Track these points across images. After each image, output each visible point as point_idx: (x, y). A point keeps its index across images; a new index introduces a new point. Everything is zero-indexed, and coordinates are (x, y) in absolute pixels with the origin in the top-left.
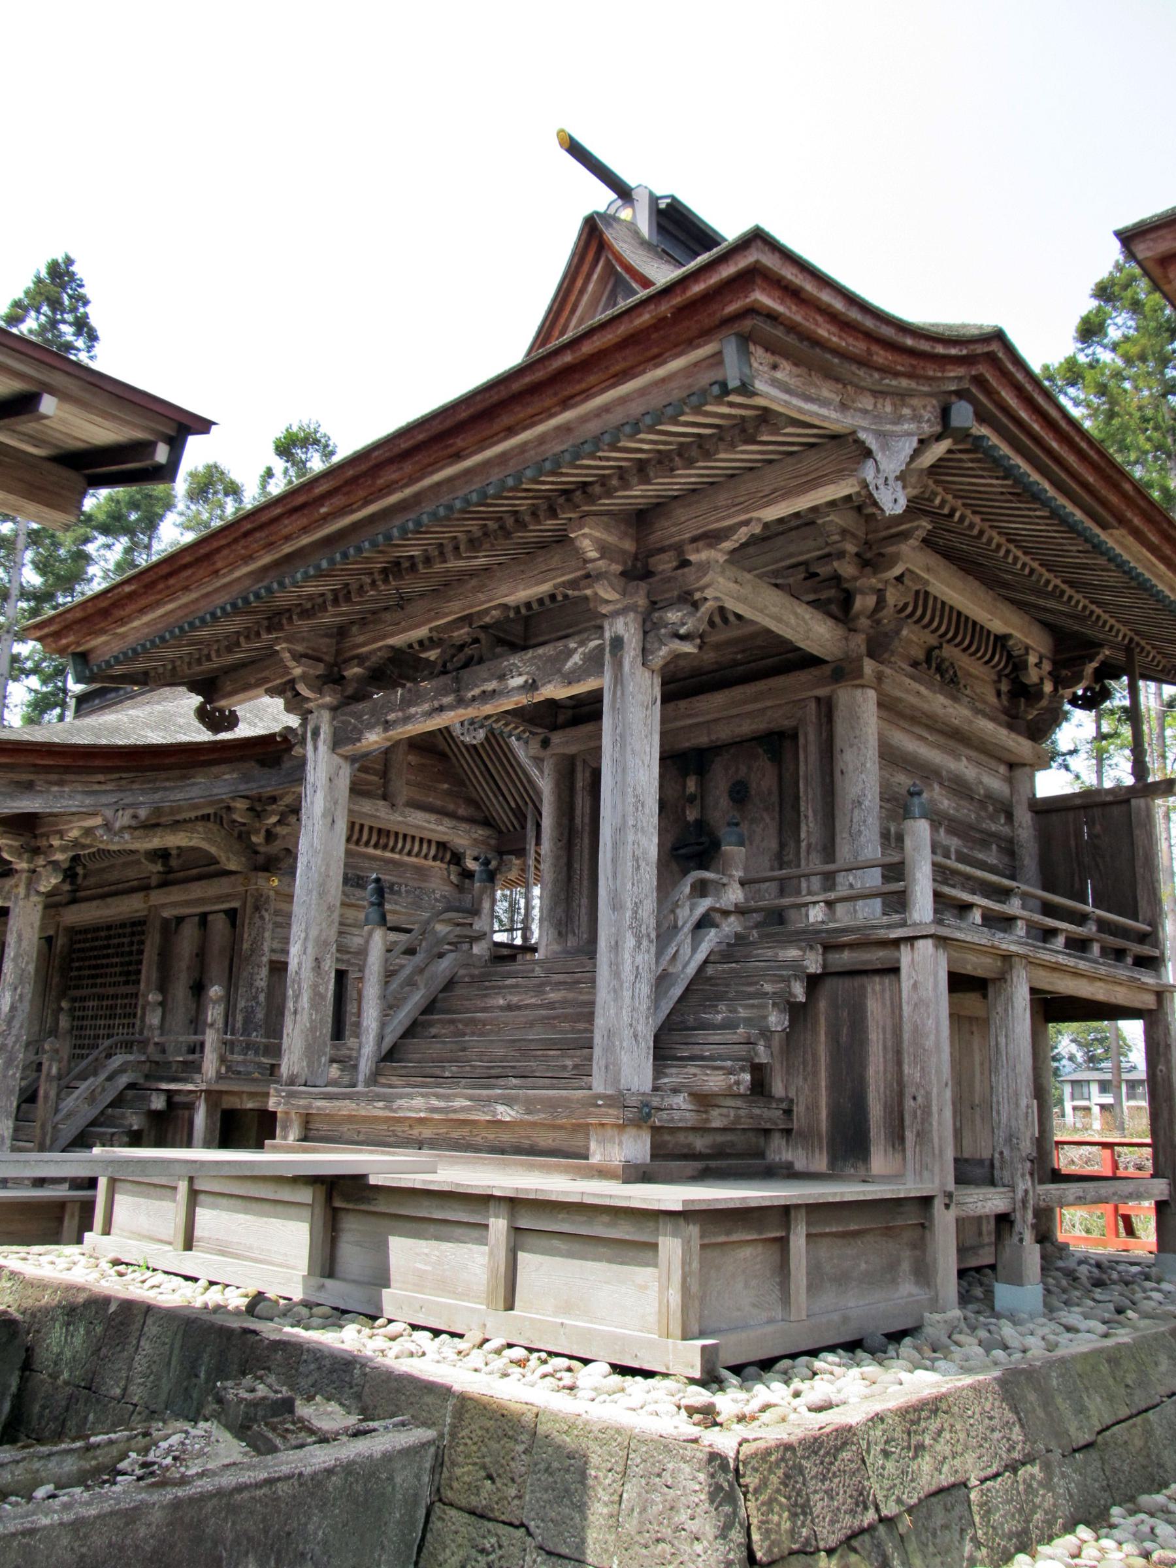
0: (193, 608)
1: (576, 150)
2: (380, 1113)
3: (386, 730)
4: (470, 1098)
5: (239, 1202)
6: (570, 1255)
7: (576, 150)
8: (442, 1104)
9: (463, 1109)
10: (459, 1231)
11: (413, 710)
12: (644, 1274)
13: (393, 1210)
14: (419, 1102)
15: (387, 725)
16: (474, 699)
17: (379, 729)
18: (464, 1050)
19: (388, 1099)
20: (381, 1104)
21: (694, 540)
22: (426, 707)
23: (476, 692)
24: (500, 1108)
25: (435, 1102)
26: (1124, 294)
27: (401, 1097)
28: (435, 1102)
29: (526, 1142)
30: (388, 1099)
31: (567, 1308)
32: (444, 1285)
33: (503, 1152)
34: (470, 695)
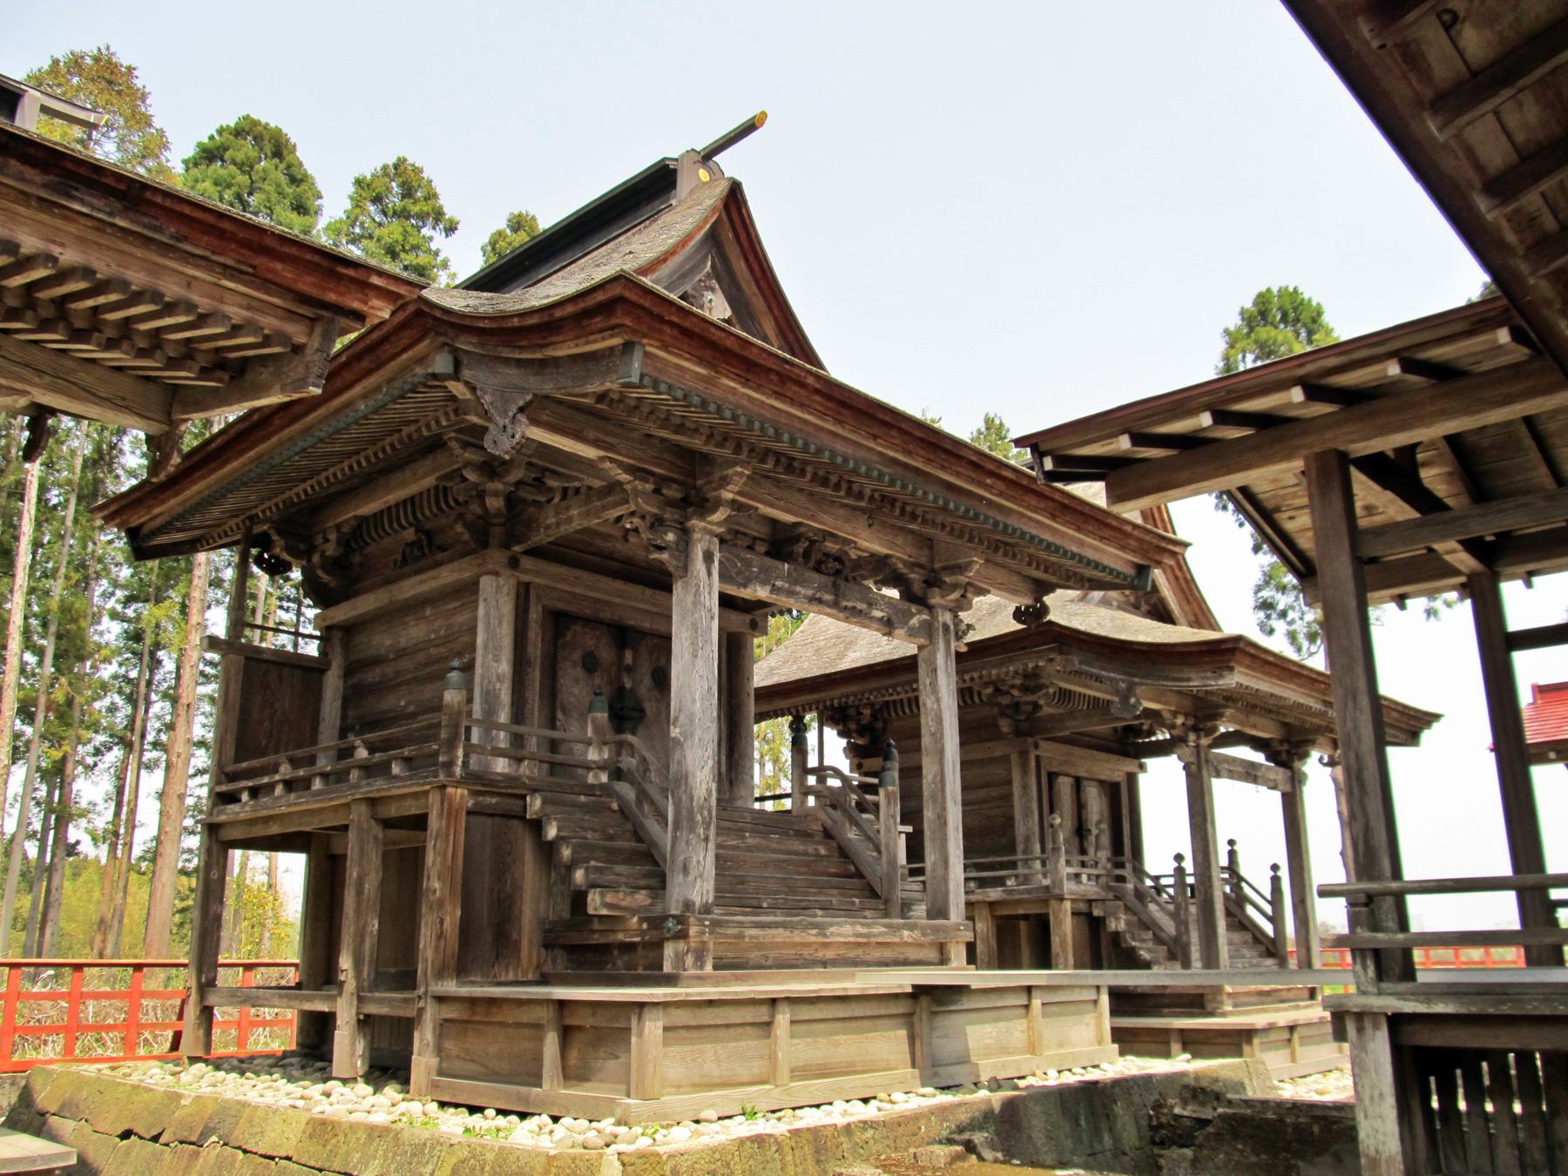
0: (811, 430)
1: (749, 128)
2: (813, 939)
3: (772, 592)
4: (885, 926)
5: (839, 1025)
6: (1060, 1014)
7: (749, 128)
8: (865, 930)
9: (880, 934)
10: (1006, 1013)
11: (798, 589)
12: (1089, 1018)
13: (999, 1004)
14: (847, 929)
15: (774, 589)
16: (846, 608)
17: (768, 588)
18: (742, 883)
19: (821, 927)
20: (814, 931)
21: (945, 569)
22: (810, 592)
23: (850, 604)
24: (906, 933)
25: (860, 929)
26: (403, 255)
27: (831, 925)
28: (860, 929)
29: (901, 957)
30: (821, 927)
31: (1061, 1045)
32: (1004, 1050)
33: (887, 965)
34: (845, 603)
